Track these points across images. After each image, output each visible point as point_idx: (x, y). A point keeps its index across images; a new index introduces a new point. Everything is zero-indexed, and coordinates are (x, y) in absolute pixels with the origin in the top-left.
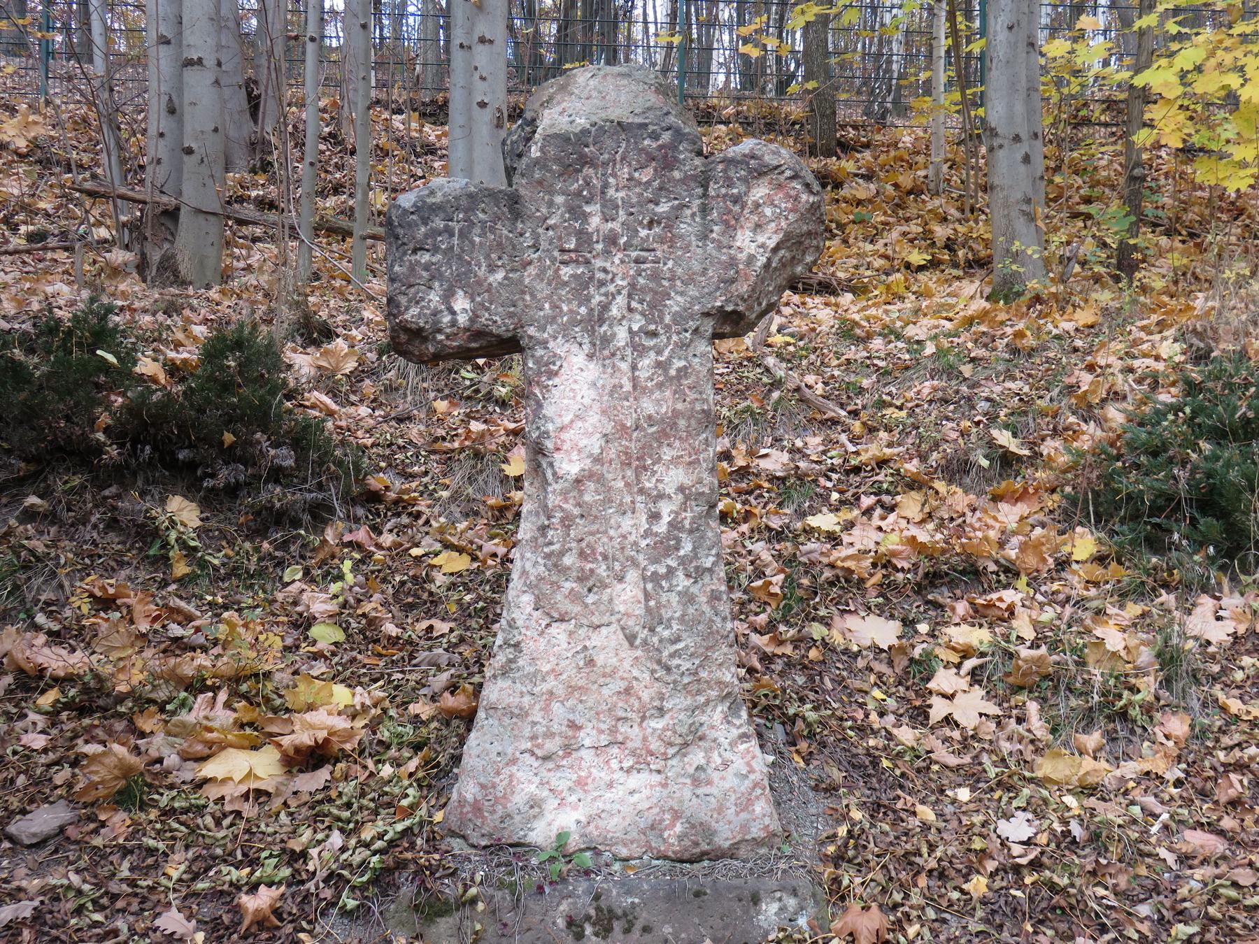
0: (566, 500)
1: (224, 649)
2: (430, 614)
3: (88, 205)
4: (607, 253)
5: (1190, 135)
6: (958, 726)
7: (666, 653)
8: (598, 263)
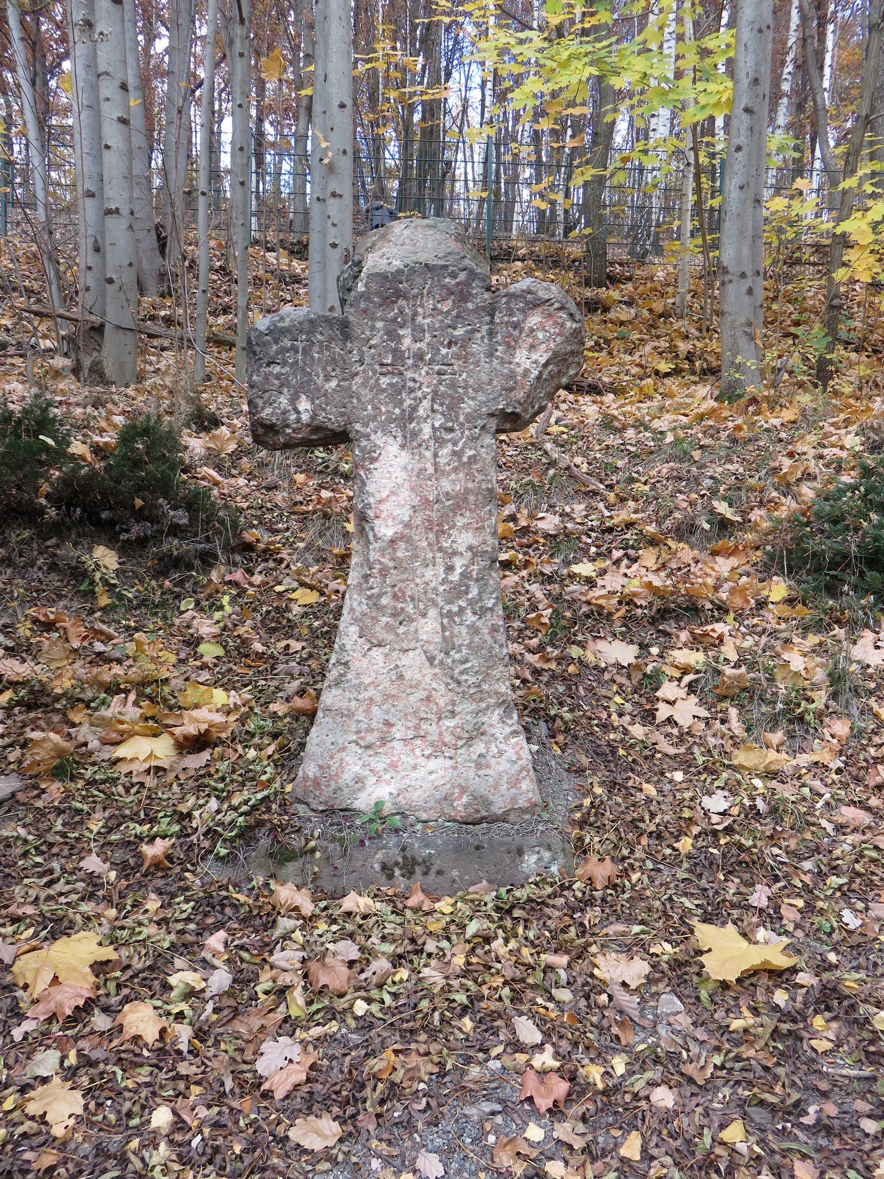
0: (383, 556)
1: (135, 661)
2: (288, 636)
3: (36, 323)
4: (416, 367)
5: (877, 274)
6: (677, 724)
7: (457, 671)
8: (409, 374)
